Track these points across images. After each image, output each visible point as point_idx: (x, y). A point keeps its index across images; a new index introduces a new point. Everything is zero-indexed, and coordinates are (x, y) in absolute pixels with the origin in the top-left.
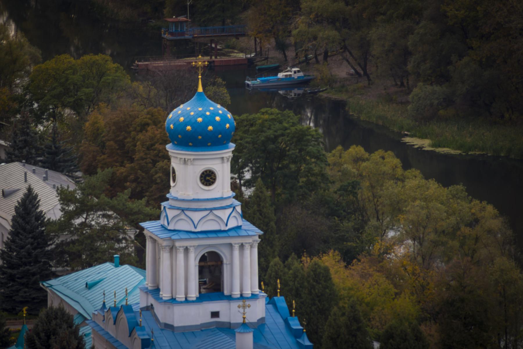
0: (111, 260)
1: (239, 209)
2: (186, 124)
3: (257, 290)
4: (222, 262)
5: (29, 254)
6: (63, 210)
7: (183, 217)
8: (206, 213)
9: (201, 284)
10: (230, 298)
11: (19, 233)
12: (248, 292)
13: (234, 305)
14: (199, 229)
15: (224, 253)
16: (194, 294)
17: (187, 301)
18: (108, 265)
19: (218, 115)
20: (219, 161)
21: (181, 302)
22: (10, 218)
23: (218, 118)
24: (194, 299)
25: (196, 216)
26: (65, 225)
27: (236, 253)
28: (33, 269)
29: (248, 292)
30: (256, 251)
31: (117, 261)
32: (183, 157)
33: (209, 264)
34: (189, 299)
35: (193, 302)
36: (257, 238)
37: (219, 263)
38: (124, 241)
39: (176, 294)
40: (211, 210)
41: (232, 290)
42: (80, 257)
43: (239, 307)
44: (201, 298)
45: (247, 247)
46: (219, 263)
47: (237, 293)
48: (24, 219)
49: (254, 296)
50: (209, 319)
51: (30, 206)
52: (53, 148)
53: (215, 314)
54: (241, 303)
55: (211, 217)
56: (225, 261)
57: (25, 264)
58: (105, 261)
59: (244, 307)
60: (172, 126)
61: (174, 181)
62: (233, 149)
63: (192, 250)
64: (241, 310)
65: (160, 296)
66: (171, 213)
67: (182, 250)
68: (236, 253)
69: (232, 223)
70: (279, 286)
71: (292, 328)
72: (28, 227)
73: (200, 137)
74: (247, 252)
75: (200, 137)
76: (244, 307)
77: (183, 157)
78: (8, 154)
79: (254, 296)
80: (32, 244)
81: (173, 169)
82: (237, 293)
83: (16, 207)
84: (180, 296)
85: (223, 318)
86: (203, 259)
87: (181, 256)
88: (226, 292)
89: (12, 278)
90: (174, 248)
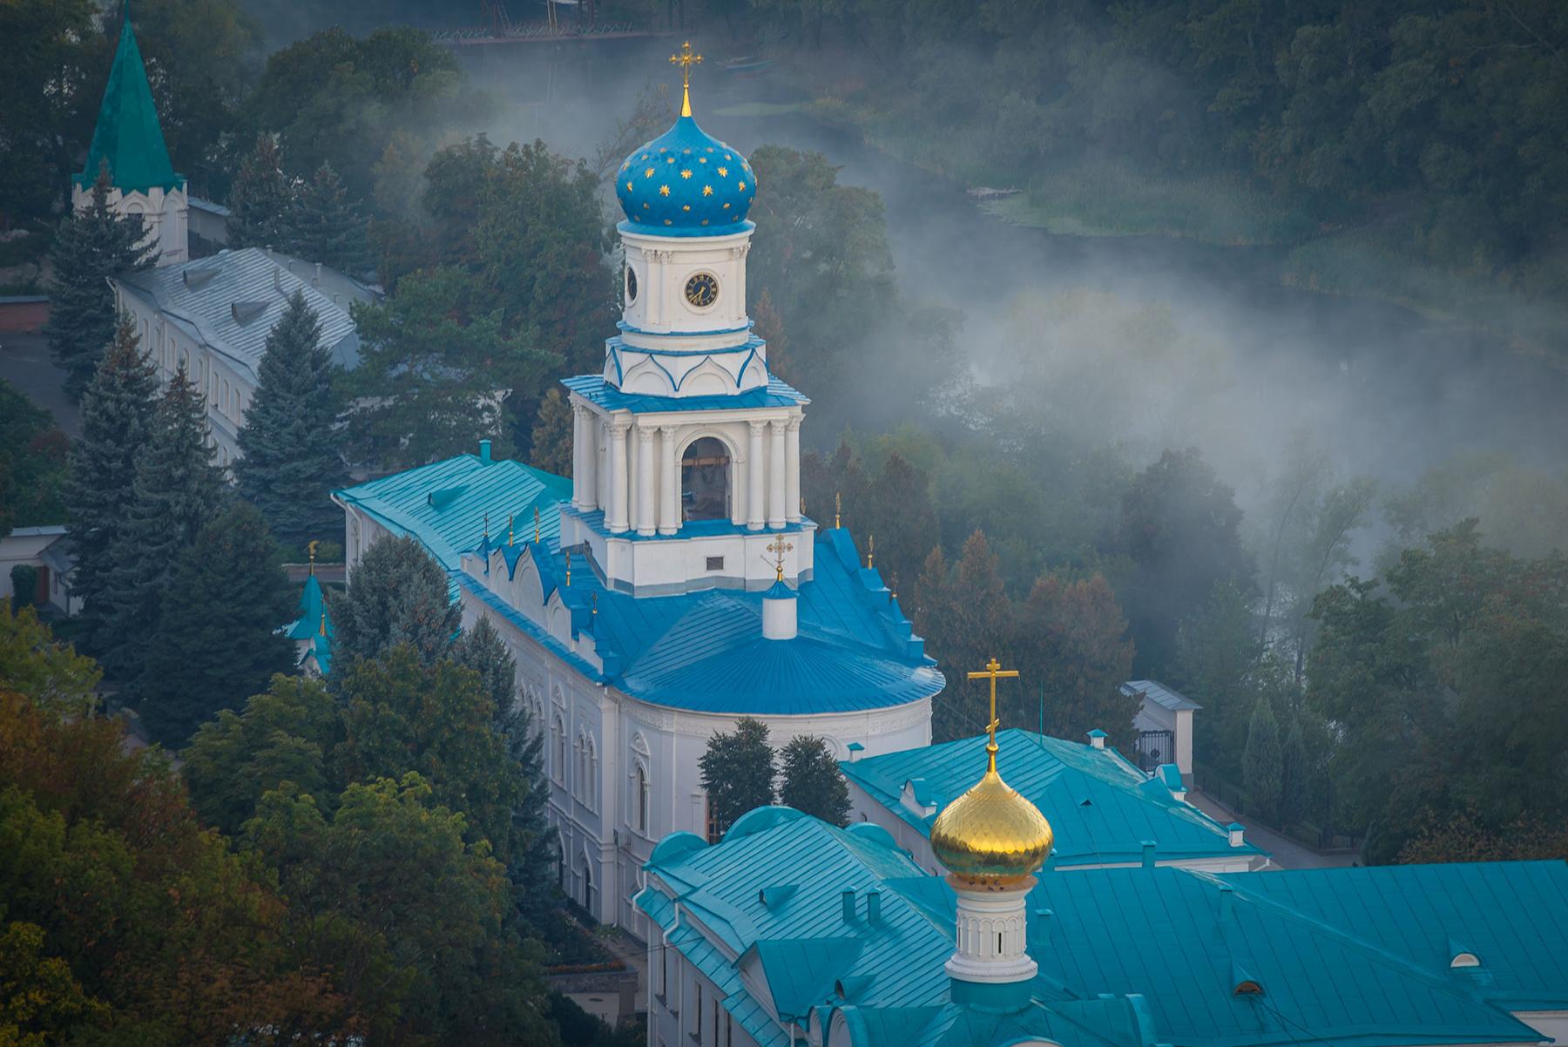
0: (476, 451)
1: (761, 352)
2: (658, 181)
3: (796, 516)
4: (728, 459)
5: (299, 437)
6: (363, 350)
7: (651, 366)
8: (701, 358)
9: (687, 501)
10: (744, 530)
11: (275, 395)
12: (778, 521)
13: (760, 544)
14: (687, 391)
15: (733, 440)
16: (672, 520)
17: (658, 535)
18: (468, 460)
19: (724, 164)
20: (725, 255)
21: (648, 538)
22: (255, 364)
23: (723, 172)
24: (674, 532)
25: (679, 367)
26: (367, 383)
27: (758, 441)
28: (309, 467)
29: (778, 521)
30: (795, 436)
31: (486, 451)
32: (654, 247)
33: (702, 462)
34: (772, 526)
35: (671, 537)
36: (798, 410)
37: (723, 461)
38: (485, 414)
39: (639, 521)
40: (651, 353)
41: (748, 513)
42: (396, 442)
43: (770, 549)
44: (684, 533)
45: (779, 429)
46: (723, 461)
47: (757, 521)
48: (288, 364)
49: (791, 527)
50: (702, 572)
51: (301, 337)
52: (324, 221)
53: (715, 563)
54: (772, 540)
55: (707, 368)
56: (734, 457)
57: (290, 458)
58: (456, 453)
59: (780, 548)
60: (630, 185)
61: (633, 294)
62: (751, 232)
63: (669, 433)
64: (774, 555)
65: (606, 526)
66: (627, 360)
67: (649, 433)
68: (758, 441)
69: (749, 383)
70: (839, 504)
71: (625, 598)
72: (297, 380)
73: (687, 208)
74: (778, 440)
75: (687, 208)
76: (780, 548)
77: (654, 247)
78: (231, 229)
79: (791, 527)
80: (304, 418)
81: (631, 273)
82: (757, 521)
83: (270, 340)
84: (647, 529)
85: (731, 570)
86: (690, 452)
87: (648, 447)
88: (736, 520)
89: (266, 485)
90: (634, 432)
